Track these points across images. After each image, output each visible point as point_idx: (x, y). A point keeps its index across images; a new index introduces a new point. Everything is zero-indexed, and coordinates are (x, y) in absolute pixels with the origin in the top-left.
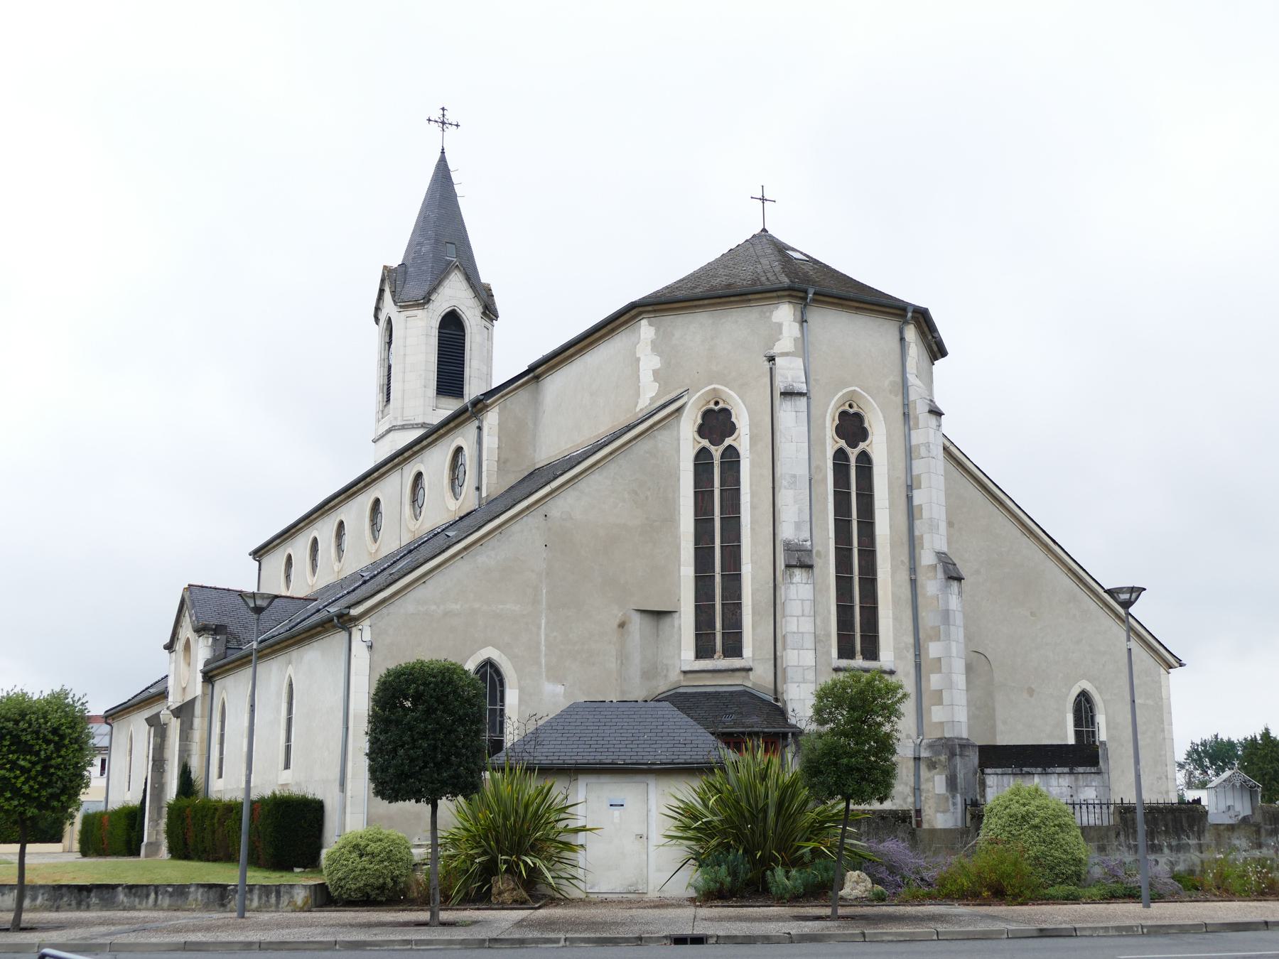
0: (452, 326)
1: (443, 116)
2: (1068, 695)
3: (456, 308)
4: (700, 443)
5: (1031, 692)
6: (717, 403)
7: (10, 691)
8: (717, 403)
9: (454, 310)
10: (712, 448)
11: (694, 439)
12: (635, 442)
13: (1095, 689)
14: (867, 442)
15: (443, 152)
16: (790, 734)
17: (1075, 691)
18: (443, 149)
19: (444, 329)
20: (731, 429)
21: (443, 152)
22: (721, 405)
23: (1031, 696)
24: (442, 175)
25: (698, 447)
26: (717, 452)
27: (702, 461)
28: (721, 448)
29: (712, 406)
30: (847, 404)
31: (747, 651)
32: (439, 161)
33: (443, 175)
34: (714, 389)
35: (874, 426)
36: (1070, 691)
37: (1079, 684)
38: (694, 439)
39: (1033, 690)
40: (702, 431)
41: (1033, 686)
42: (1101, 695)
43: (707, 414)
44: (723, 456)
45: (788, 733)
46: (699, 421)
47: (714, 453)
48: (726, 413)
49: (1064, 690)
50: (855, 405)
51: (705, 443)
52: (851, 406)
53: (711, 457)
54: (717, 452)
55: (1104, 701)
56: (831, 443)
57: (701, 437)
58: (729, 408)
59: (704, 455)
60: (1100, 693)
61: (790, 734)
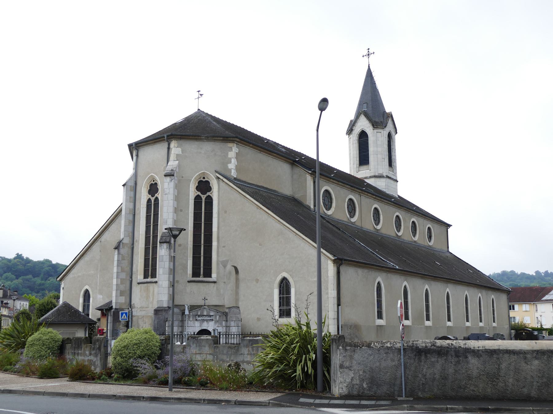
0: (390, 136)
1: (371, 54)
2: (275, 280)
3: (363, 129)
4: (197, 193)
5: (257, 281)
6: (154, 181)
7: (307, 322)
8: (154, 181)
9: (363, 130)
10: (202, 196)
11: (195, 191)
12: (237, 192)
13: (289, 276)
14: (211, 192)
15: (369, 67)
16: (104, 310)
17: (279, 278)
18: (369, 65)
19: (360, 139)
20: (209, 189)
21: (369, 67)
22: (206, 179)
23: (257, 283)
24: (369, 75)
25: (148, 198)
26: (204, 197)
27: (197, 200)
28: (205, 196)
29: (202, 179)
30: (202, 178)
31: (214, 275)
32: (368, 70)
33: (369, 75)
34: (152, 175)
35: (214, 185)
36: (276, 278)
37: (281, 274)
38: (195, 191)
39: (258, 280)
40: (198, 188)
41: (258, 278)
42: (292, 278)
43: (200, 182)
44: (206, 199)
45: (103, 309)
46: (149, 188)
47: (205, 197)
48: (207, 182)
49: (273, 278)
50: (206, 178)
51: (199, 193)
52: (204, 178)
53: (201, 199)
54: (204, 197)
55: (294, 281)
56: (193, 193)
57: (197, 191)
58: (209, 181)
59: (198, 198)
60: (292, 278)
61: (104, 310)
